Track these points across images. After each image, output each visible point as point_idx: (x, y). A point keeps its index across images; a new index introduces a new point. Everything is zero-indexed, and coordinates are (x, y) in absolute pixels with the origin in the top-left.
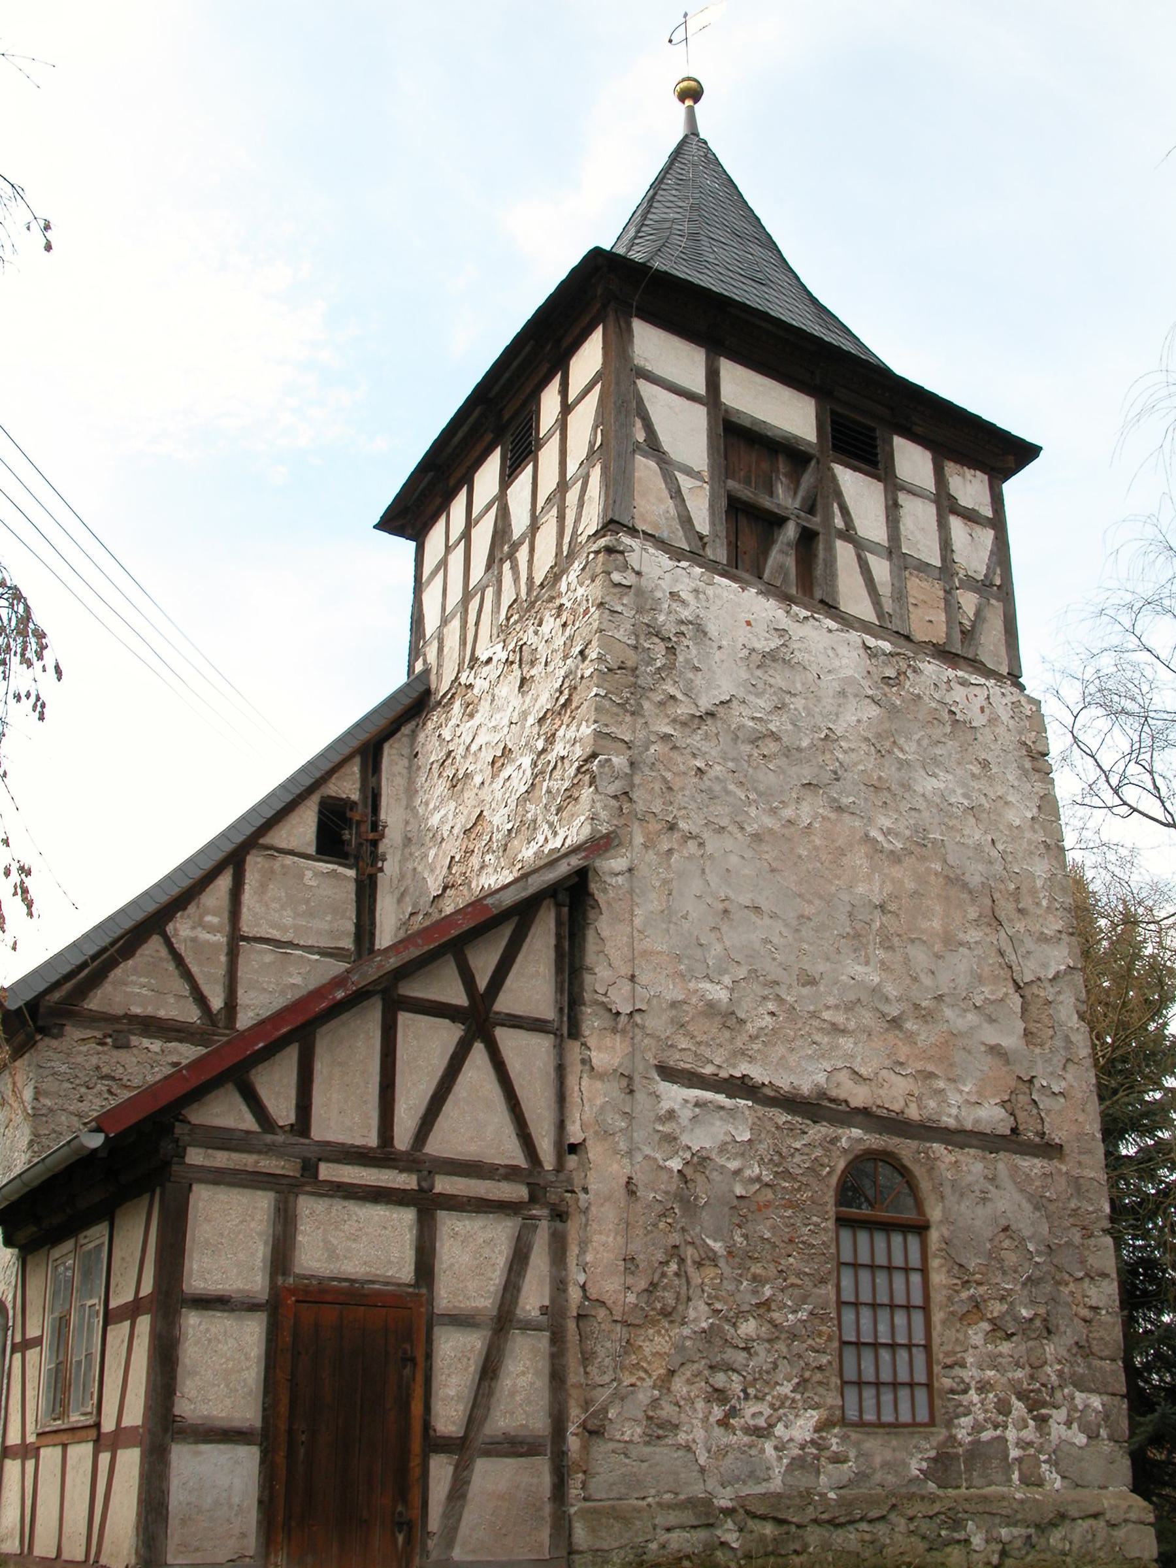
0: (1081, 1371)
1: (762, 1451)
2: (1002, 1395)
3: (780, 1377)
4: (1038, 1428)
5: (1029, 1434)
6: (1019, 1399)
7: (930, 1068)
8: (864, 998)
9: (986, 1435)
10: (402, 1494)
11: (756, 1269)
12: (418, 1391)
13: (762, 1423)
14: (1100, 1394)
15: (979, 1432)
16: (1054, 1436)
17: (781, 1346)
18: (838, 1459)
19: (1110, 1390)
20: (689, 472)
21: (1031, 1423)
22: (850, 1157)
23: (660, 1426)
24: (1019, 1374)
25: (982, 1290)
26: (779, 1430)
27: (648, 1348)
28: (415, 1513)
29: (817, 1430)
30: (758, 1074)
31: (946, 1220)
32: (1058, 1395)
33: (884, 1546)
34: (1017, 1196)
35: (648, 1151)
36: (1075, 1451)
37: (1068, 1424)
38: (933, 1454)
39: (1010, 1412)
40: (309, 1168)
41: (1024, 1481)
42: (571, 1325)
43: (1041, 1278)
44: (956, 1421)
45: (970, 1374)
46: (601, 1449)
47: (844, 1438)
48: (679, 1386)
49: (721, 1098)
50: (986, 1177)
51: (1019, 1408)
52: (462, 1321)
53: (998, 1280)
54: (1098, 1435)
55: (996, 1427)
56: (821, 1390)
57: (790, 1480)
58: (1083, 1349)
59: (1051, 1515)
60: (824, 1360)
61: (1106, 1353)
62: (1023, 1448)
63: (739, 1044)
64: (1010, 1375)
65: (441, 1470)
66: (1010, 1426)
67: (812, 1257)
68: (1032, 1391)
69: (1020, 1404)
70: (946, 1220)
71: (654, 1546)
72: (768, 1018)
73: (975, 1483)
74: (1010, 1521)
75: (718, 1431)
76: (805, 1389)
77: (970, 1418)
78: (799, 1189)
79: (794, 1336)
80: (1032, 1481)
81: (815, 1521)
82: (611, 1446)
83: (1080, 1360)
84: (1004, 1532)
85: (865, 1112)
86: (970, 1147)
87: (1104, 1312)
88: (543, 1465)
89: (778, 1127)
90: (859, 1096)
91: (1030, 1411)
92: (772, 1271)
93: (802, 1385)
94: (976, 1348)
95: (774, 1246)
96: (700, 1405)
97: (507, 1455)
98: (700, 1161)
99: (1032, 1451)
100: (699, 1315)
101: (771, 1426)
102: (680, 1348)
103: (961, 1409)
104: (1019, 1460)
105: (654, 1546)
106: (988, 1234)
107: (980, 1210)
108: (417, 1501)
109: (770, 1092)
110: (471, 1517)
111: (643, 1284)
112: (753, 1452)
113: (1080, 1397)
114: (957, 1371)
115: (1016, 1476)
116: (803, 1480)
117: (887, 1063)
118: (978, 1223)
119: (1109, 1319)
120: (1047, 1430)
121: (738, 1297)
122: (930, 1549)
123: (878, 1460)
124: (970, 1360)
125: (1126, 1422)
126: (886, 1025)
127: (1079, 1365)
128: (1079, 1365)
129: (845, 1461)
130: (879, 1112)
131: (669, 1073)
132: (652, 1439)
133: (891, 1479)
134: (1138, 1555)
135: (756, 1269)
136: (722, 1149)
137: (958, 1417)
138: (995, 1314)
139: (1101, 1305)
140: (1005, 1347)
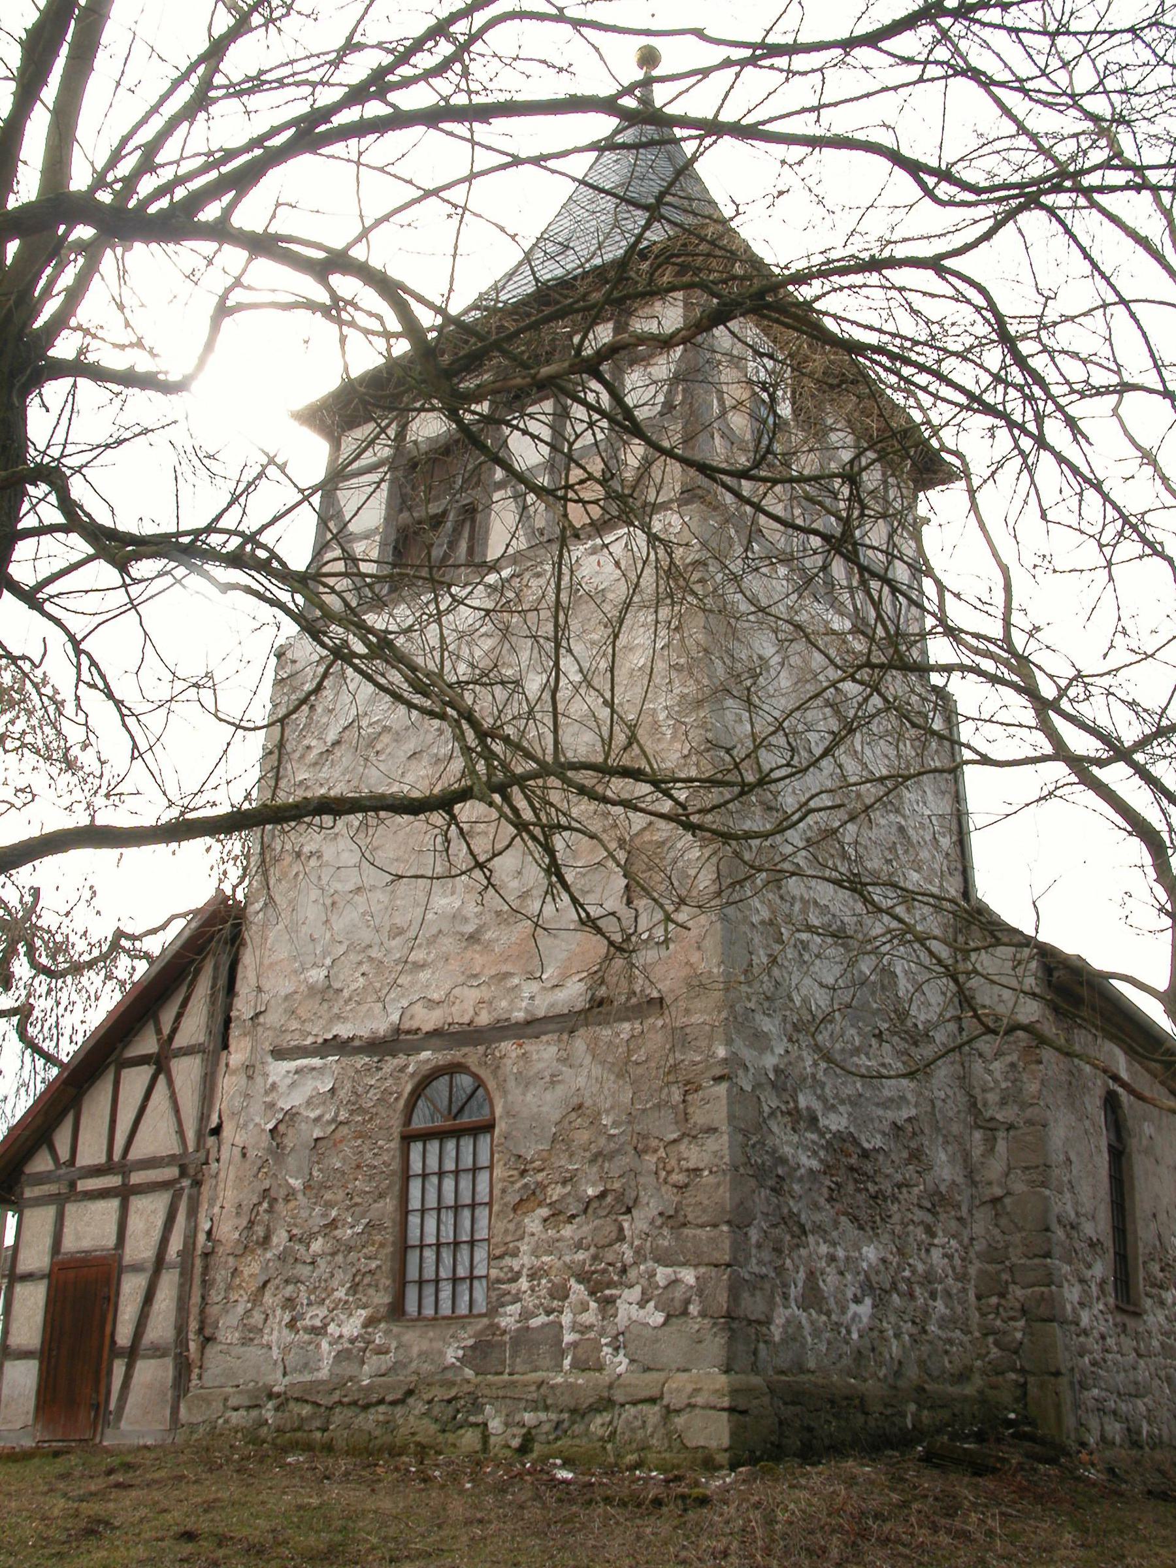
0: (666, 1243)
1: (318, 1346)
2: (557, 1280)
3: (335, 1283)
4: (602, 1311)
5: (589, 1317)
6: (579, 1282)
7: (505, 968)
8: (445, 927)
9: (535, 1322)
10: (97, 1382)
11: (328, 1196)
12: (110, 1316)
13: (318, 1323)
14: (696, 1266)
15: (527, 1319)
16: (622, 1320)
17: (339, 1258)
18: (382, 1351)
19: (706, 1260)
20: (617, 132)
21: (593, 1305)
22: (416, 1079)
23: (250, 1331)
24: (581, 1256)
25: (540, 1177)
26: (331, 1328)
27: (246, 1273)
28: (102, 1398)
29: (365, 1325)
30: (344, 1030)
31: (508, 1113)
32: (633, 1274)
33: (398, 1426)
34: (597, 1071)
35: (257, 1120)
36: (647, 1332)
37: (642, 1304)
38: (471, 1342)
39: (567, 1297)
40: (72, 1185)
41: (580, 1366)
42: (198, 1263)
43: (618, 1151)
44: (501, 1310)
45: (525, 1260)
46: (212, 1351)
47: (387, 1332)
48: (268, 1299)
49: (316, 1062)
50: (558, 1060)
51: (578, 1290)
52: (136, 1268)
53: (562, 1163)
54: (685, 1313)
55: (548, 1313)
56: (371, 1291)
57: (338, 1370)
58: (673, 1220)
59: (591, 1400)
60: (373, 1265)
61: (704, 1219)
62: (582, 1333)
63: (336, 1010)
64: (567, 1259)
65: (119, 1368)
66: (566, 1310)
67: (371, 1178)
68: (594, 1272)
69: (582, 1287)
70: (508, 1113)
71: (221, 1421)
72: (361, 979)
73: (517, 1369)
74: (534, 1406)
75: (285, 1331)
76: (355, 1293)
77: (518, 1305)
78: (371, 1119)
79: (350, 1249)
80: (588, 1364)
81: (340, 1403)
82: (220, 1347)
83: (665, 1231)
84: (528, 1417)
85: (436, 1033)
86: (545, 1033)
87: (706, 1173)
88: (169, 1362)
89: (357, 1071)
90: (427, 1020)
91: (592, 1293)
92: (341, 1195)
93: (354, 1288)
94: (533, 1235)
95: (344, 1173)
96: (279, 1312)
97: (152, 1357)
98: (291, 1116)
99: (592, 1335)
100: (280, 1239)
101: (326, 1326)
102: (265, 1268)
103: (508, 1298)
104: (575, 1345)
105: (221, 1421)
106: (556, 1116)
107: (549, 1096)
108: (103, 1391)
109: (357, 1043)
110: (132, 1399)
111: (245, 1223)
112: (312, 1347)
113: (663, 1274)
114: (508, 1261)
115: (567, 1362)
116: (349, 1369)
117: (461, 979)
118: (544, 1109)
119: (712, 1180)
120: (612, 1312)
121: (310, 1222)
122: (444, 1431)
123: (415, 1351)
124: (524, 1248)
125: (725, 1295)
126: (464, 944)
127: (664, 1237)
128: (664, 1237)
129: (387, 1353)
130: (452, 1029)
131: (279, 1054)
132: (246, 1342)
133: (426, 1367)
134: (702, 1443)
135: (328, 1196)
136: (309, 1103)
137: (503, 1305)
138: (555, 1198)
139: (701, 1165)
140: (567, 1231)
